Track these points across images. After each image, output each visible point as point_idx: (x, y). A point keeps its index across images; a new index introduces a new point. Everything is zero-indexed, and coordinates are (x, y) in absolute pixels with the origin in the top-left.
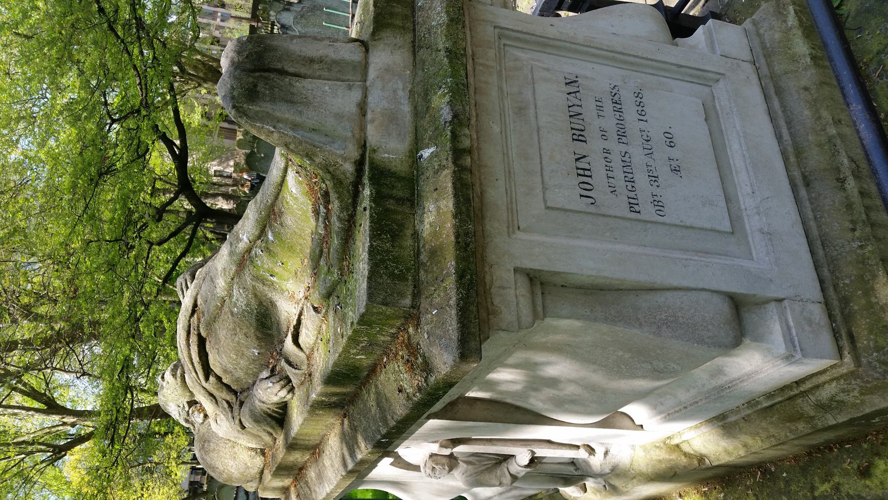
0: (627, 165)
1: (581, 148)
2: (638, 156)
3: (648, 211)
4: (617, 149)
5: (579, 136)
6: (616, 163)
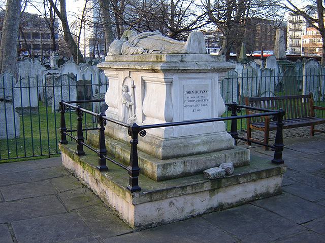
0: (193, 101)
1: (195, 92)
2: (195, 103)
3: (186, 104)
4: (196, 99)
5: (197, 92)
6: (194, 99)
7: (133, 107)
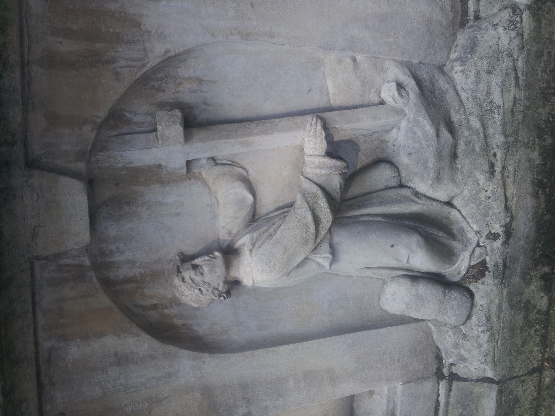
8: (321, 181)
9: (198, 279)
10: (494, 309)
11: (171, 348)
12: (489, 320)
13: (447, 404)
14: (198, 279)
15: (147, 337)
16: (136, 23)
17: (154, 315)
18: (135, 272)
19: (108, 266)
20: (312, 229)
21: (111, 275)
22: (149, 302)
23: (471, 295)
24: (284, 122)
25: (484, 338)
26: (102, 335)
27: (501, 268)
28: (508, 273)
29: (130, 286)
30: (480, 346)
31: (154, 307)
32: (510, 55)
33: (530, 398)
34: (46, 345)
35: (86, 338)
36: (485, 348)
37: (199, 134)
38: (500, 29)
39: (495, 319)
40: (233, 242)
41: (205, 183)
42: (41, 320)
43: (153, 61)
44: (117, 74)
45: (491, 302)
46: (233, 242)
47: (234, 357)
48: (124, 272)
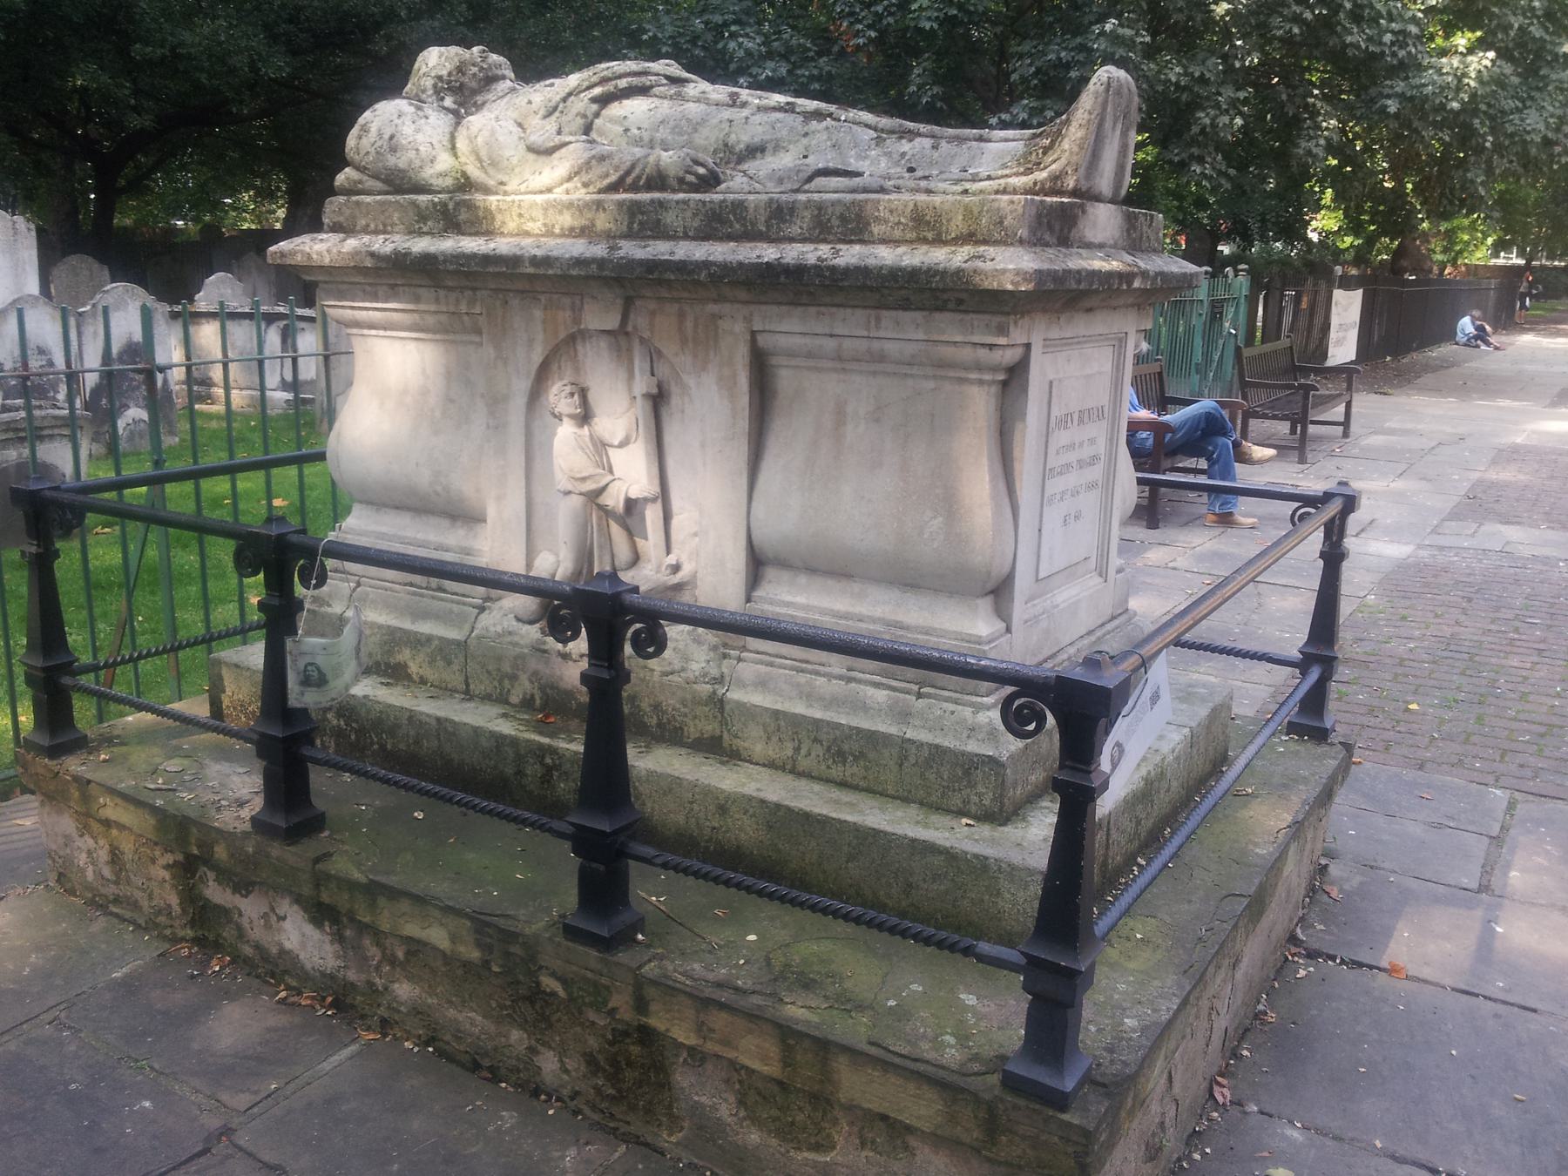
7: (652, 515)
8: (610, 489)
9: (563, 394)
10: (516, 639)
11: (533, 375)
12: (510, 633)
13: (464, 604)
14: (563, 394)
15: (541, 360)
16: (704, 369)
17: (555, 367)
18: (580, 356)
19: (584, 339)
20: (578, 476)
21: (579, 341)
22: (563, 364)
23: (531, 623)
24: (655, 470)
25: (499, 629)
26: (545, 331)
27: (543, 647)
28: (539, 654)
29: (572, 353)
30: (494, 625)
31: (560, 368)
32: (683, 669)
33: (448, 679)
34: (543, 298)
35: (544, 322)
36: (492, 629)
37: (648, 406)
38: (704, 665)
39: (509, 639)
40: (589, 424)
41: (628, 410)
42: (556, 296)
43: (685, 377)
44: (677, 354)
45: (522, 637)
46: (589, 424)
47: (522, 419)
48: (579, 347)
